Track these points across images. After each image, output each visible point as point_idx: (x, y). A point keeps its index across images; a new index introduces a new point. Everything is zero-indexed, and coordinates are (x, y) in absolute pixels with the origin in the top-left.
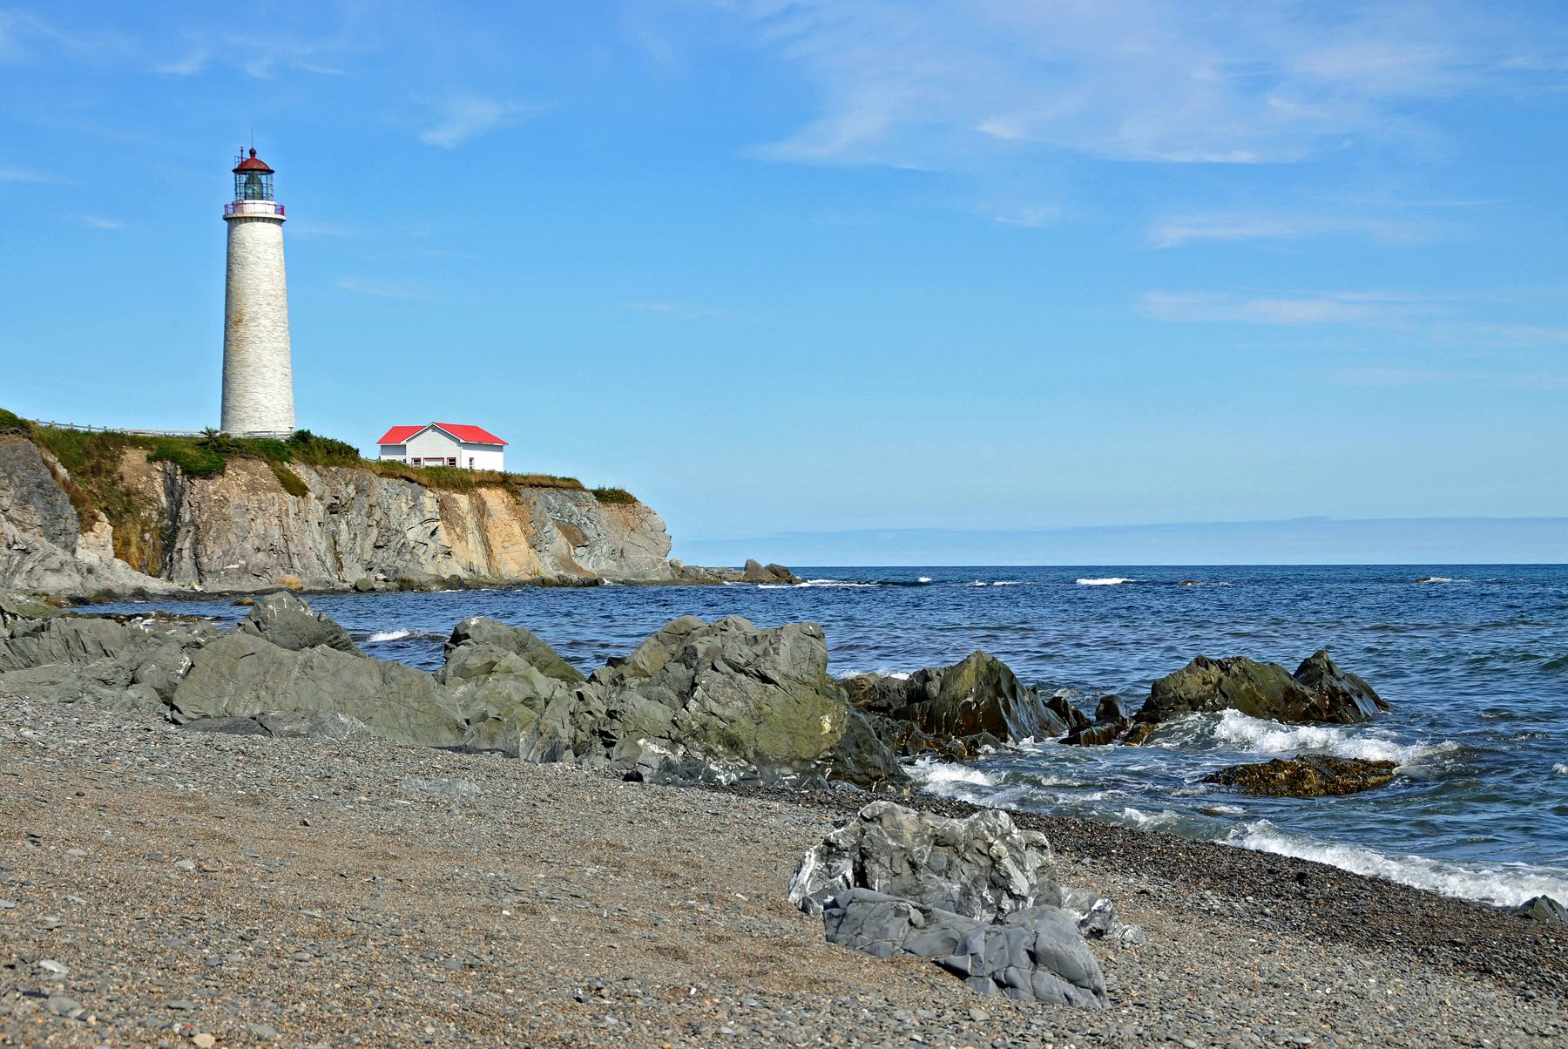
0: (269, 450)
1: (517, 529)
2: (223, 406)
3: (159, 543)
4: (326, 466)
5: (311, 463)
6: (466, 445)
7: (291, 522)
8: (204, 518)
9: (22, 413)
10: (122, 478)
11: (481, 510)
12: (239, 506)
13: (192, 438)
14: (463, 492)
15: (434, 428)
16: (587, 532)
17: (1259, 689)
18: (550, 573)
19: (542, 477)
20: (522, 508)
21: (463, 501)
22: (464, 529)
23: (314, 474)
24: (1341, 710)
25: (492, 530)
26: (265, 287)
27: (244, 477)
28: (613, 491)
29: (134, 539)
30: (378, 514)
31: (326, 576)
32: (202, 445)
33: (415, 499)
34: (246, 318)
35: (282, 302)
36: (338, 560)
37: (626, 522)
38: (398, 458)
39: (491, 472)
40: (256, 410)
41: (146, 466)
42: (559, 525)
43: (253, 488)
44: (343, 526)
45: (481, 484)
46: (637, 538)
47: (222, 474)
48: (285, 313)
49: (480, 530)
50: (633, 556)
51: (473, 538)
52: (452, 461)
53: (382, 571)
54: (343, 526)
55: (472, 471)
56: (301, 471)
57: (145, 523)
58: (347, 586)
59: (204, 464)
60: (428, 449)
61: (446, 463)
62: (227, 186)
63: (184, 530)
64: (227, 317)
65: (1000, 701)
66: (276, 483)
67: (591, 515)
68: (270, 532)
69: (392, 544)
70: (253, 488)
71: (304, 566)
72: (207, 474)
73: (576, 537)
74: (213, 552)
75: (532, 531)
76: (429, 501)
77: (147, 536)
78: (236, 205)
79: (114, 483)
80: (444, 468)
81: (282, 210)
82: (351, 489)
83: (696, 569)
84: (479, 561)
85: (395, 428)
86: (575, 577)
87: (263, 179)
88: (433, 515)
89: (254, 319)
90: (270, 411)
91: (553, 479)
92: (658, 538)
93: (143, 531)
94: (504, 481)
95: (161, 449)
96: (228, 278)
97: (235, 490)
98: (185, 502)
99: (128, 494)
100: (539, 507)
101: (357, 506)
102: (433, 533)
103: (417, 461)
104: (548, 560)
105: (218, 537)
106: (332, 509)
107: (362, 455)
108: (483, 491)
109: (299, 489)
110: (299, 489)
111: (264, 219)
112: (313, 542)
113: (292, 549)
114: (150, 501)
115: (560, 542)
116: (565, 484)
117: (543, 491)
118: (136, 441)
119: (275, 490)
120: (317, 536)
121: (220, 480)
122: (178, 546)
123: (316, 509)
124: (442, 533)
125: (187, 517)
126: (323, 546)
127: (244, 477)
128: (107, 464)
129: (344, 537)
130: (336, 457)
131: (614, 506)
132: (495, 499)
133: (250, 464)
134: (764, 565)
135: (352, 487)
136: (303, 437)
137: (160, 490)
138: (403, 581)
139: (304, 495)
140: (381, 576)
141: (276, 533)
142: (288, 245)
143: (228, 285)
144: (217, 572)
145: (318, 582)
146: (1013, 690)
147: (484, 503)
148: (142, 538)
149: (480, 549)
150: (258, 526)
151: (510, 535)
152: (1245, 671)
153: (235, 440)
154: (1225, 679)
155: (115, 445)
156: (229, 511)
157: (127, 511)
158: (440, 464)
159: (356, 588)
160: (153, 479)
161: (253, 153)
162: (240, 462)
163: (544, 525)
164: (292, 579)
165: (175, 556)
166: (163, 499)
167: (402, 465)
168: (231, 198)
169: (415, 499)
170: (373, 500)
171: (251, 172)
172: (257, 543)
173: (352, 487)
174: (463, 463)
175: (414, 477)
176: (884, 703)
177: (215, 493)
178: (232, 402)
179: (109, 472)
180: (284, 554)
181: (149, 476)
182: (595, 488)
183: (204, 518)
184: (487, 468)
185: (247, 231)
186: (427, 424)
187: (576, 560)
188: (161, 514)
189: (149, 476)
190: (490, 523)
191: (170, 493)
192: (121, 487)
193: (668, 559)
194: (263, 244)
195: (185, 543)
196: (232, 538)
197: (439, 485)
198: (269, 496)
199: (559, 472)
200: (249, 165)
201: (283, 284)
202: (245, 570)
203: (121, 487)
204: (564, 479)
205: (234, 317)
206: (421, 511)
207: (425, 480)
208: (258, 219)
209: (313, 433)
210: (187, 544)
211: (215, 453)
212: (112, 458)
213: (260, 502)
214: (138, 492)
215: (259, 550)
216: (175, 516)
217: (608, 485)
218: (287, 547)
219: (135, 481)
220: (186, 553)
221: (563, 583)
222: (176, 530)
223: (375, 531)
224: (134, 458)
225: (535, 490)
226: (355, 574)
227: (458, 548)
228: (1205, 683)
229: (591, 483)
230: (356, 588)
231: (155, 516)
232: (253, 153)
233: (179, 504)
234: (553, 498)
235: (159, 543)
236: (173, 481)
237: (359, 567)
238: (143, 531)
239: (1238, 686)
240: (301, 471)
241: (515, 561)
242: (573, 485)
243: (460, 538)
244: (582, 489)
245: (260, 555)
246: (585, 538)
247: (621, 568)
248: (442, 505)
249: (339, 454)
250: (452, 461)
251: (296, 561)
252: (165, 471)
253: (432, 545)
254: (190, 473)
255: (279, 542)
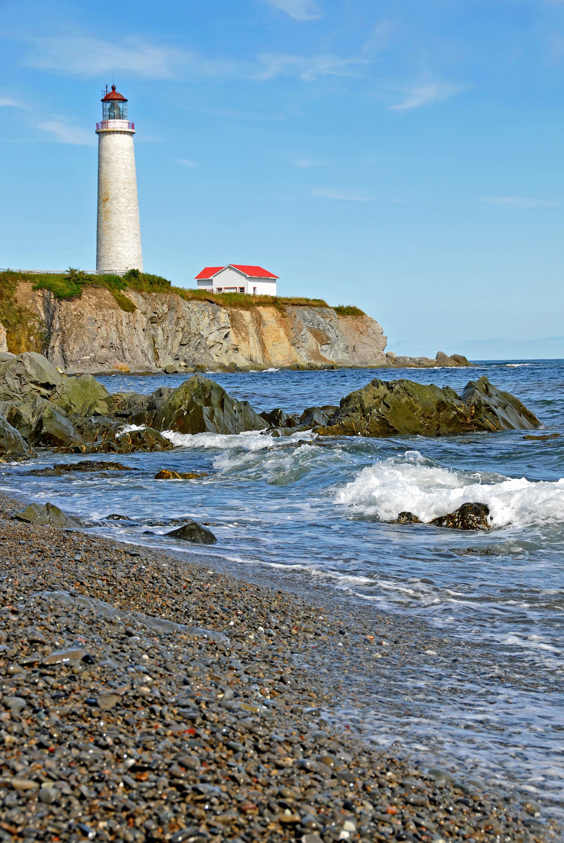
0: (113, 282)
1: (282, 333)
2: (97, 256)
3: (40, 342)
4: (149, 292)
5: (139, 291)
6: (251, 279)
7: (124, 328)
8: (68, 326)
9: (15, 268)
10: (16, 301)
11: (259, 321)
12: (90, 319)
13: (63, 275)
14: (247, 309)
15: (230, 267)
16: (329, 335)
17: (416, 401)
18: (303, 360)
19: (301, 299)
20: (286, 319)
21: (247, 315)
22: (247, 334)
23: (141, 298)
24: (481, 416)
25: (266, 334)
26: (122, 177)
27: (94, 300)
28: (349, 308)
29: (24, 340)
30: (182, 323)
31: (147, 364)
32: (68, 279)
33: (214, 314)
34: (111, 197)
35: (133, 186)
36: (156, 353)
37: (357, 329)
38: (208, 288)
39: (266, 296)
40: (118, 258)
41: (32, 293)
42: (311, 330)
43: (99, 307)
44: (160, 331)
45: (259, 304)
46: (364, 339)
47: (80, 297)
48: (135, 194)
49: (258, 334)
50: (361, 350)
51: (253, 339)
52: (242, 289)
53: (185, 361)
54: (160, 331)
55: (254, 296)
56: (132, 296)
57: (30, 330)
58: (160, 370)
59: (68, 291)
60: (228, 281)
61: (238, 291)
62: (97, 110)
63: (55, 334)
64: (99, 197)
65: (206, 410)
66: (115, 303)
67: (332, 323)
68: (111, 335)
69: (192, 343)
70: (99, 307)
71: (132, 357)
72: (70, 298)
73: (322, 338)
74: (73, 349)
75: (292, 334)
76: (223, 315)
77: (32, 338)
78: (104, 123)
79: (11, 304)
80: (235, 294)
81: (132, 126)
82: (165, 307)
83: (404, 359)
84: (257, 354)
85: (206, 268)
86: (319, 364)
87: (121, 105)
88: (226, 325)
89: (115, 199)
90: (126, 255)
91: (307, 300)
92: (378, 338)
93: (29, 335)
94: (274, 302)
95: (41, 282)
96: (99, 172)
97: (88, 309)
98: (56, 317)
99: (20, 311)
100: (298, 319)
101: (169, 318)
102: (226, 336)
103: (220, 289)
104: (303, 353)
105: (77, 339)
106: (152, 320)
107: (173, 284)
108: (260, 309)
109: (130, 308)
110: (130, 308)
111: (121, 132)
112: (141, 341)
113: (125, 346)
114: (34, 315)
115: (311, 342)
116: (315, 303)
117: (301, 308)
118: (25, 277)
119: (114, 308)
120: (142, 338)
121: (78, 302)
122: (52, 344)
123: (142, 320)
124: (232, 336)
125: (57, 326)
126: (146, 344)
127: (94, 300)
128: (7, 292)
129: (160, 338)
130: (156, 287)
131: (349, 318)
132: (268, 314)
133: (98, 291)
134: (449, 355)
135: (166, 306)
136: (134, 273)
137: (41, 309)
138: (198, 367)
139: (133, 311)
140: (183, 364)
141: (114, 336)
142: (138, 151)
143: (99, 176)
144: (76, 361)
145: (141, 368)
146: (222, 404)
147: (261, 317)
148: (29, 339)
149: (258, 346)
150: (103, 332)
151: (278, 337)
152: (405, 389)
153: (88, 276)
154: (389, 395)
155: (12, 280)
156: (84, 322)
157: (19, 322)
158: (233, 291)
159: (165, 371)
160: (35, 302)
161: (114, 88)
162: (92, 290)
163: (301, 330)
164: (123, 366)
165: (50, 351)
166: (43, 314)
167: (210, 293)
168: (100, 119)
169: (214, 314)
170: (179, 315)
171: (113, 100)
172: (102, 342)
173: (166, 306)
174: (249, 291)
175: (213, 300)
176: (127, 412)
177: (75, 310)
178: (103, 253)
179: (8, 297)
180: (120, 350)
181: (33, 300)
182: (337, 306)
183: (68, 326)
184: (264, 294)
185: (110, 140)
186: (225, 265)
187: (322, 353)
188: (41, 324)
189: (33, 300)
190: (264, 329)
191: (47, 310)
192: (15, 307)
193: (385, 352)
194: (121, 147)
195: (56, 343)
196: (86, 340)
197: (231, 305)
198: (110, 312)
199: (312, 296)
200: (112, 97)
201: (134, 175)
202: (93, 360)
203: (15, 307)
204: (315, 300)
205: (103, 197)
206: (218, 322)
207: (221, 302)
208: (117, 132)
209: (141, 271)
210: (57, 344)
211: (75, 284)
212: (10, 288)
213: (104, 316)
214: (26, 310)
215: (103, 347)
216: (50, 326)
217: (345, 304)
218: (121, 345)
219: (24, 303)
220: (56, 349)
221: (312, 368)
222: (50, 334)
223: (180, 335)
224: (24, 287)
225: (296, 308)
226: (166, 362)
227: (243, 346)
228: (374, 398)
229: (333, 303)
230: (165, 371)
231: (37, 325)
232: (114, 88)
233: (53, 318)
234: (307, 313)
235: (40, 342)
236: (49, 303)
237: (169, 358)
238: (29, 335)
239: (399, 400)
240: (132, 296)
241: (281, 353)
242: (321, 304)
243: (244, 339)
244: (327, 306)
245: (104, 350)
246: (328, 338)
247: (354, 358)
248: (232, 318)
249: (158, 284)
250: (242, 289)
251: (127, 354)
252: (44, 296)
253: (225, 344)
254: (59, 297)
255: (116, 342)
